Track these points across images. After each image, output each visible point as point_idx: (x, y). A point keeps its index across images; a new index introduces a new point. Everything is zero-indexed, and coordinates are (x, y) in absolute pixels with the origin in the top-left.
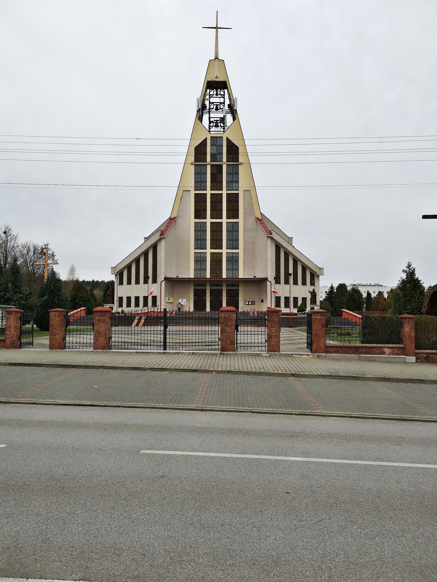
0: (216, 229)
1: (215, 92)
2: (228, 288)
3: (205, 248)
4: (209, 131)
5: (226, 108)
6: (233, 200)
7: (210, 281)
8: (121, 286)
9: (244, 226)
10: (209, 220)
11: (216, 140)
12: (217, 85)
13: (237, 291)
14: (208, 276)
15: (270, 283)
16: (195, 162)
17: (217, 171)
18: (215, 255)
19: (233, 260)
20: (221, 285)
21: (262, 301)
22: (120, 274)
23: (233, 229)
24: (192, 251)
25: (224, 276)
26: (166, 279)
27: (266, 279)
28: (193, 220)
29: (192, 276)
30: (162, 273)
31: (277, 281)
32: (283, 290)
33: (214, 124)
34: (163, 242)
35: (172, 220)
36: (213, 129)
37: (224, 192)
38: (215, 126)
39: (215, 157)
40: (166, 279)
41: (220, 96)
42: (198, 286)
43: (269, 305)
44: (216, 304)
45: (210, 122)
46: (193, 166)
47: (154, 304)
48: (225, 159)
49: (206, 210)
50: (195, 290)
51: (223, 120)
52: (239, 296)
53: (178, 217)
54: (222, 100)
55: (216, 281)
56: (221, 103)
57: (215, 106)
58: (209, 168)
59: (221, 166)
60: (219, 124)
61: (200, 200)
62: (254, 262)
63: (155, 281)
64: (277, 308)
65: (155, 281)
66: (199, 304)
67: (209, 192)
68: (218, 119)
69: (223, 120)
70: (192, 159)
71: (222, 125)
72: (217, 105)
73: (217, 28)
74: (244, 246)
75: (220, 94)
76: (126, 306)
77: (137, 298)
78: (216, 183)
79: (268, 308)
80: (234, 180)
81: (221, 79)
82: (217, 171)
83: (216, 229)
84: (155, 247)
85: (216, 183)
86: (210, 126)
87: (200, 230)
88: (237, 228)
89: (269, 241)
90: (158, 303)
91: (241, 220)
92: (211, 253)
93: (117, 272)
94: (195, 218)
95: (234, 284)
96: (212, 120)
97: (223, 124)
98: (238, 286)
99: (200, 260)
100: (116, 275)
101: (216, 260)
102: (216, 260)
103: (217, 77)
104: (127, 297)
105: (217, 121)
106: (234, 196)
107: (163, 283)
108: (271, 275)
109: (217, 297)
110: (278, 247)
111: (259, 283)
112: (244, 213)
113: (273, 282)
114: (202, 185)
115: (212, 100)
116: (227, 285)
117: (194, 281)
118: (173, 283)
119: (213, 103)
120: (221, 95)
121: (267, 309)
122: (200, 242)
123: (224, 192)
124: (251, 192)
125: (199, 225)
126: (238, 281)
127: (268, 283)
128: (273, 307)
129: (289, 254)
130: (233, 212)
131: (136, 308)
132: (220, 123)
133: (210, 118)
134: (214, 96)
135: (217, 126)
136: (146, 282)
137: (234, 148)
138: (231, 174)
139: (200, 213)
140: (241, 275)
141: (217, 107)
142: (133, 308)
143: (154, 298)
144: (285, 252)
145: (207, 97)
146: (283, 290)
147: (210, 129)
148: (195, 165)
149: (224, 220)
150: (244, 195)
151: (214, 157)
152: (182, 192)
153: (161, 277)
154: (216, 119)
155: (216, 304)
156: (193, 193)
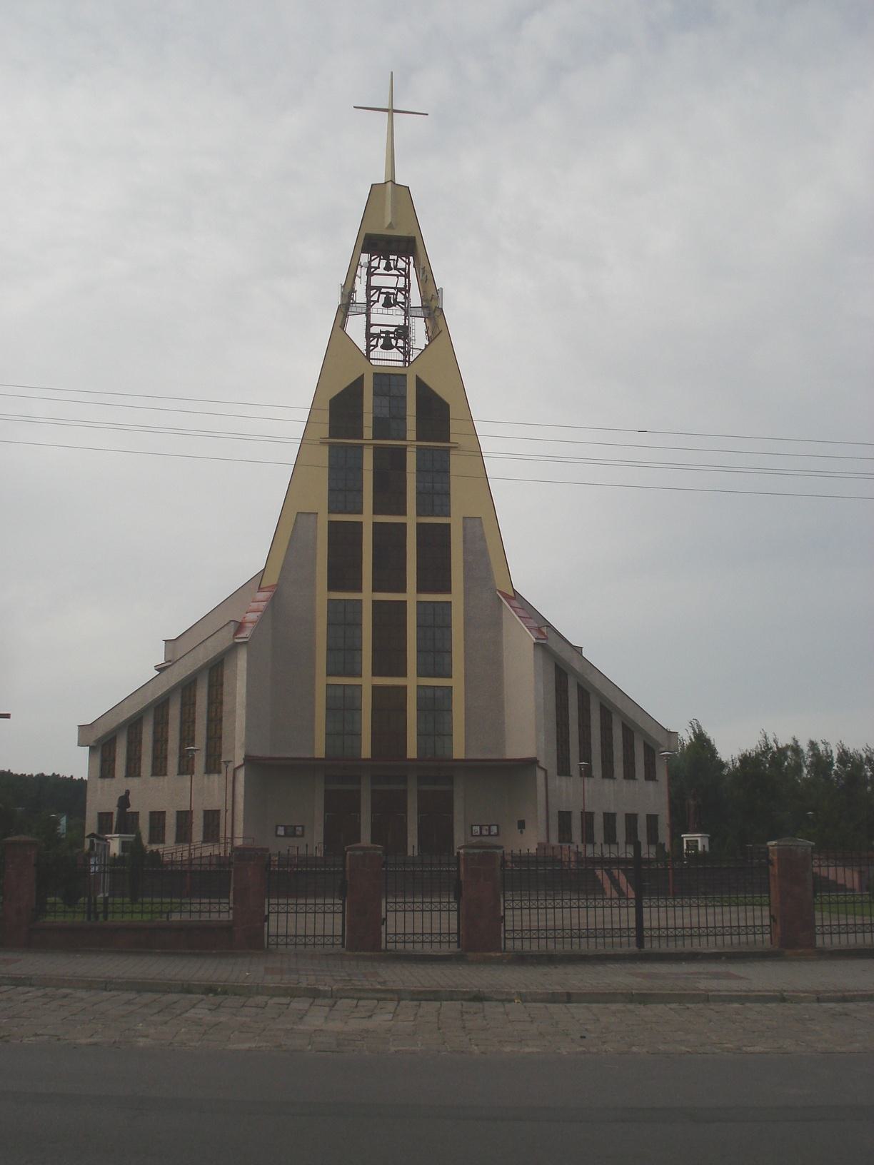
0: (390, 618)
1: (383, 263)
3: (359, 674)
6: (435, 543)
8: (107, 781)
10: (367, 596)
11: (388, 383)
12: (390, 238)
14: (366, 752)
16: (331, 436)
17: (389, 466)
19: (436, 705)
21: (522, 825)
24: (322, 681)
25: (412, 752)
29: (320, 752)
31: (564, 770)
32: (573, 793)
33: (381, 341)
36: (378, 353)
37: (411, 520)
39: (388, 424)
40: (249, 760)
41: (396, 272)
45: (369, 336)
46: (326, 449)
47: (211, 832)
48: (411, 434)
49: (360, 491)
51: (403, 332)
52: (456, 811)
54: (401, 284)
56: (400, 290)
57: (383, 297)
58: (368, 432)
59: (403, 451)
60: (394, 342)
61: (343, 541)
63: (213, 765)
66: (340, 827)
68: (392, 329)
70: (324, 431)
71: (401, 343)
72: (387, 293)
73: (391, 111)
75: (396, 268)
78: (389, 496)
80: (436, 495)
82: (389, 466)
83: (390, 618)
84: (216, 669)
85: (389, 496)
86: (368, 346)
87: (343, 619)
93: (98, 741)
95: (440, 773)
96: (374, 330)
99: (341, 706)
100: (92, 749)
101: (389, 702)
102: (389, 702)
104: (152, 813)
107: (241, 775)
113: (553, 770)
115: (375, 281)
119: (379, 289)
120: (398, 270)
122: (343, 657)
127: (540, 775)
128: (554, 841)
133: (369, 325)
134: (381, 271)
135: (387, 346)
139: (343, 573)
140: (459, 752)
141: (387, 299)
142: (599, 849)
144: (580, 687)
145: (362, 272)
146: (573, 793)
147: (368, 351)
148: (332, 446)
149: (411, 596)
151: (381, 428)
154: (384, 329)
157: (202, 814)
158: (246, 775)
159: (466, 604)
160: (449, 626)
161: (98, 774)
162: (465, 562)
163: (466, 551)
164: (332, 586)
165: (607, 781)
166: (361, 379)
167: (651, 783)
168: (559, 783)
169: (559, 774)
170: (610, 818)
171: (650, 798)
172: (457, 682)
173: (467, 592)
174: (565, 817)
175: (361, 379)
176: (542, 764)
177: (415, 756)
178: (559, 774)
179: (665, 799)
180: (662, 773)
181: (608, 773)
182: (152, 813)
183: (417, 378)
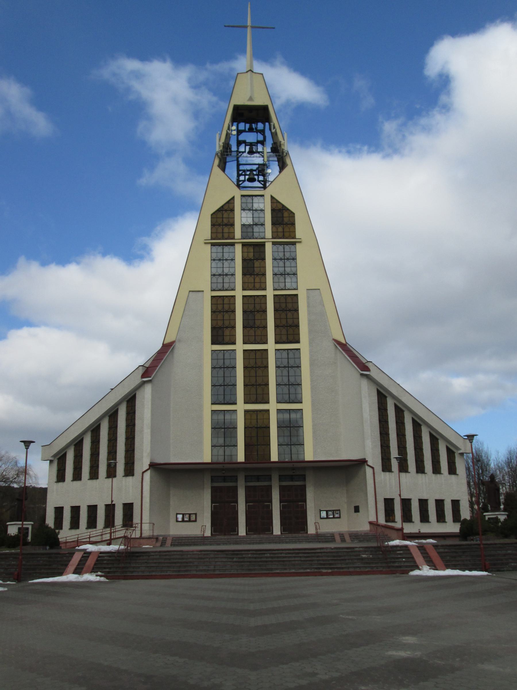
0: (256, 363)
2: (284, 484)
4: (238, 186)
5: (268, 149)
6: (287, 307)
7: (245, 469)
8: (60, 484)
9: (311, 356)
10: (240, 347)
13: (303, 489)
14: (241, 457)
15: (371, 470)
18: (254, 417)
19: (291, 428)
20: (269, 478)
21: (357, 509)
22: (60, 459)
23: (290, 365)
24: (208, 407)
25: (274, 457)
26: (153, 466)
27: (363, 462)
28: (208, 347)
29: (207, 458)
30: (145, 454)
31: (386, 467)
34: (148, 389)
35: (167, 348)
38: (249, 153)
40: (153, 466)
42: (218, 477)
43: (373, 519)
44: (259, 523)
48: (269, 233)
50: (214, 490)
51: (262, 170)
52: (308, 501)
53: (180, 341)
54: (261, 138)
55: (258, 470)
57: (248, 148)
58: (238, 248)
61: (222, 308)
62: (333, 426)
64: (390, 524)
65: (129, 471)
67: (239, 293)
68: (255, 167)
69: (262, 170)
74: (312, 397)
76: (69, 527)
77: (92, 510)
79: (371, 523)
80: (287, 272)
81: (259, 101)
83: (256, 363)
84: (131, 400)
87: (222, 367)
88: (232, 306)
89: (365, 383)
90: (136, 519)
91: (304, 345)
92: (246, 412)
93: (54, 456)
94: (213, 343)
95: (297, 476)
96: (241, 168)
97: (264, 175)
98: (303, 478)
99: (223, 429)
100: (51, 462)
103: (251, 99)
104: (72, 507)
105: (251, 171)
106: (289, 300)
107: (147, 476)
108: (372, 454)
109: (258, 486)
110: (382, 396)
111: (347, 471)
112: (310, 332)
113: (378, 467)
114: (259, 332)
115: (242, 137)
116: (281, 478)
117: (212, 470)
118: (170, 474)
121: (366, 528)
122: (223, 392)
123: (270, 293)
124: (321, 293)
125: (221, 356)
126: (304, 469)
128: (382, 521)
129: (386, 397)
130: (288, 330)
131: (90, 530)
132: (258, 175)
133: (238, 165)
136: (111, 473)
137: (286, 214)
138: (281, 259)
139: (221, 333)
140: (309, 455)
143: (128, 508)
150: (308, 297)
152: (186, 294)
153: (142, 462)
155: (259, 523)
156: (208, 295)
157: (103, 508)
158: (151, 477)
159: (311, 351)
160: (297, 326)
161: (55, 479)
162: (309, 321)
163: (309, 313)
164: (214, 342)
165: (420, 475)
166: (233, 198)
167: (453, 476)
168: (383, 477)
169: (383, 470)
170: (423, 503)
171: (454, 488)
172: (306, 406)
173: (311, 342)
174: (389, 503)
175: (233, 198)
176: (370, 463)
177: (276, 459)
178: (383, 470)
179: (464, 488)
180: (460, 466)
181: (420, 469)
182: (72, 507)
183: (272, 196)
